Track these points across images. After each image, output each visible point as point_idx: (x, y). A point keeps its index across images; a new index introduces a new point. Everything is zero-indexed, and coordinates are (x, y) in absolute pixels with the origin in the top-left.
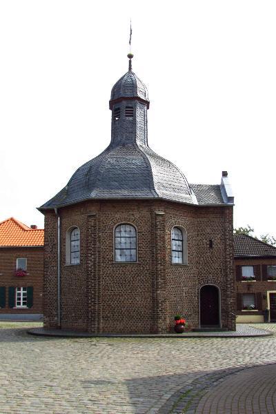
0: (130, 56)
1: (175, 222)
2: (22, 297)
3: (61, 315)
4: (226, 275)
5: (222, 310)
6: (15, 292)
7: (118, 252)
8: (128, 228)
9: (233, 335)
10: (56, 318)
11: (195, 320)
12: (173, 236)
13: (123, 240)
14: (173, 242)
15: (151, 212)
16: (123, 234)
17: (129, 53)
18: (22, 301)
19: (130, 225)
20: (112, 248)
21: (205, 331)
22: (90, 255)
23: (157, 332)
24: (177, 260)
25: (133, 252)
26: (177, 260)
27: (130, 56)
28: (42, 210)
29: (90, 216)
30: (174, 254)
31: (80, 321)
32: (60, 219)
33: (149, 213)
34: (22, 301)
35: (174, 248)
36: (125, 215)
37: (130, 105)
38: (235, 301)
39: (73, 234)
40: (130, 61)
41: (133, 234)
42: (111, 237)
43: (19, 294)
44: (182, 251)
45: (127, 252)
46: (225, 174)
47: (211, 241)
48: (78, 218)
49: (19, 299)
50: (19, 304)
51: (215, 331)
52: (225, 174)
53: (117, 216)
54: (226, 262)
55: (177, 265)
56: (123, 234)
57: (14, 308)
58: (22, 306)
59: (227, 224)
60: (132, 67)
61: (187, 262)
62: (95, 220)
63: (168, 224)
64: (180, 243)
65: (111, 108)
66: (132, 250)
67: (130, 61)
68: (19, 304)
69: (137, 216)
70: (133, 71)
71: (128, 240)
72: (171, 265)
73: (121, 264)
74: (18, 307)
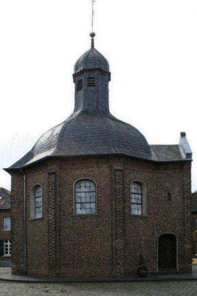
0: (93, 35)
1: (135, 177)
2: (9, 248)
3: (27, 262)
4: (184, 224)
5: (180, 255)
6: (3, 244)
7: (78, 206)
8: (88, 184)
9: (190, 277)
10: (23, 265)
11: (153, 265)
12: (133, 190)
13: (83, 195)
14: (133, 196)
15: (111, 167)
16: (83, 189)
17: (91, 32)
18: (9, 251)
19: (92, 181)
20: (72, 202)
21: (165, 274)
22: (50, 209)
23: (144, 276)
24: (136, 211)
25: (93, 205)
26: (136, 211)
27: (93, 35)
28: (8, 170)
29: (50, 174)
30: (133, 207)
31: (43, 267)
32: (26, 177)
33: (108, 169)
34: (9, 251)
35: (134, 201)
36: (84, 171)
37: (92, 76)
38: (191, 247)
39: (37, 191)
40: (93, 40)
41: (93, 188)
42: (72, 192)
43: (7, 246)
44: (141, 204)
45: (87, 206)
46: (183, 135)
47: (169, 194)
48: (40, 177)
49: (7, 249)
50: (7, 253)
51: (172, 274)
52: (183, 135)
53: (77, 172)
54: (184, 212)
55: (136, 216)
56: (83, 189)
57: (3, 256)
58: (9, 255)
59: (185, 178)
60: (95, 44)
61: (145, 214)
62: (55, 177)
63: (127, 180)
64: (140, 196)
65: (75, 82)
66: (92, 204)
67: (93, 40)
68: (7, 253)
69: (96, 171)
70: (95, 47)
71: (88, 195)
72: (130, 216)
73: (81, 217)
74: (6, 255)
